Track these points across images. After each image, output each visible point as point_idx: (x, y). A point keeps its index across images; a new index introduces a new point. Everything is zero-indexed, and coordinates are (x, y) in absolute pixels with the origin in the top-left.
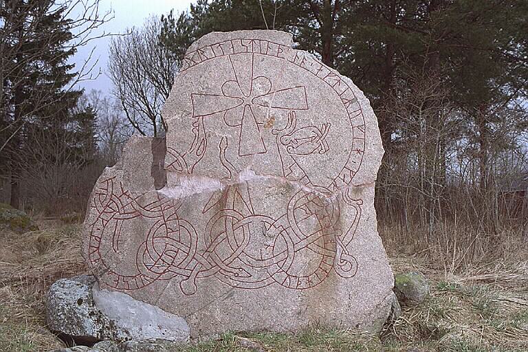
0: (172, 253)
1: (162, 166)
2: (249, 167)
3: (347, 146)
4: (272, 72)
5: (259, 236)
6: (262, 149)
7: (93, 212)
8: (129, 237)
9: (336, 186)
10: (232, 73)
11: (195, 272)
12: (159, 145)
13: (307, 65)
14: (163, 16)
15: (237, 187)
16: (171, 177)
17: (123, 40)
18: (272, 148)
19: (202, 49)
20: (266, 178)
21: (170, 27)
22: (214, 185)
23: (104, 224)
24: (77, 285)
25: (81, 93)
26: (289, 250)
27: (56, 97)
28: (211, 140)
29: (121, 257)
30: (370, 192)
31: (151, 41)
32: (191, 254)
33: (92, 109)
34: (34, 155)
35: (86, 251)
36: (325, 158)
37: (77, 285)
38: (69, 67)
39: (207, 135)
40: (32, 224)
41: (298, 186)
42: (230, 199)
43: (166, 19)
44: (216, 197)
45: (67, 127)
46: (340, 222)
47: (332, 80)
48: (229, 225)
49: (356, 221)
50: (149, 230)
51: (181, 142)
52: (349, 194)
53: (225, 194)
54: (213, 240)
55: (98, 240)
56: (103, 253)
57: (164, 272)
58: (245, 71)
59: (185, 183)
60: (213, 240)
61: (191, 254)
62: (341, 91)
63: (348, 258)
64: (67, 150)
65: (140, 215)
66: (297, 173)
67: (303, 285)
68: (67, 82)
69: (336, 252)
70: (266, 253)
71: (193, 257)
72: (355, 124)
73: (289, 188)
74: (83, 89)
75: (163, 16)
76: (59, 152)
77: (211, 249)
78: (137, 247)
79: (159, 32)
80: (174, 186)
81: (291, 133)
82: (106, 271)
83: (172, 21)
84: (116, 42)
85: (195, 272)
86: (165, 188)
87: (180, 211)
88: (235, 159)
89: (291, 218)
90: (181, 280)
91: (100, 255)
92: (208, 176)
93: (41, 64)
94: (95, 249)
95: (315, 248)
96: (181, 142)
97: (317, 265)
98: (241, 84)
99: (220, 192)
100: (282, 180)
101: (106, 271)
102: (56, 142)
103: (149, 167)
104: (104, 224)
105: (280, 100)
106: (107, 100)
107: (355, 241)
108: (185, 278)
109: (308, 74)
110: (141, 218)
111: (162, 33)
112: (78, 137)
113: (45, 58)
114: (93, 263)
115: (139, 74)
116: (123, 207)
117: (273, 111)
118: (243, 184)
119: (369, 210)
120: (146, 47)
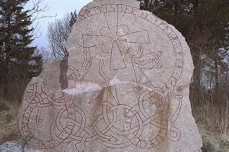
0: (71, 128)
1: (66, 76)
2: (116, 77)
3: (173, 64)
4: (129, 23)
5: (122, 117)
6: (123, 66)
7: (25, 103)
8: (46, 119)
9: (167, 87)
10: (106, 23)
11: (84, 138)
12: (64, 65)
13: (149, 18)
14: (72, 13)
15: (109, 88)
16: (71, 82)
17: (54, 24)
18: (129, 65)
19: (89, 10)
20: (126, 83)
21: (75, 18)
22: (96, 87)
23: (31, 110)
24: (16, 145)
25: (36, 48)
26: (140, 125)
27: (24, 49)
28: (94, 61)
29: (40, 129)
30: (187, 91)
31: (66, 24)
32: (82, 128)
33: (41, 55)
34: (14, 75)
35: (20, 126)
36: (160, 71)
37: (16, 145)
38: (31, 36)
39: (92, 58)
40: (7, 107)
41: (145, 88)
42: (105, 95)
43: (73, 14)
44: (97, 94)
45: (30, 63)
46: (170, 109)
47: (163, 27)
48: (105, 111)
49: (179, 108)
50: (57, 113)
51: (76, 62)
52: (175, 92)
53: (102, 92)
54: (95, 119)
55: (28, 119)
56: (30, 127)
57: (66, 138)
58: (113, 22)
59: (79, 85)
60: (95, 119)
61: (82, 128)
62: (168, 33)
63: (175, 130)
64: (29, 73)
65: (52, 105)
66: (144, 80)
67: (149, 146)
68: (30, 43)
69: (168, 126)
70: (127, 127)
71: (83, 129)
72: (177, 51)
73: (139, 88)
74: (37, 46)
75: (72, 13)
76: (25, 74)
77: (94, 125)
78: (50, 123)
79: (70, 20)
80: (72, 88)
81: (141, 57)
82: (32, 138)
83: (76, 15)
84: (51, 24)
85: (84, 138)
86: (67, 89)
87: (76, 102)
88: (108, 72)
89: (141, 106)
90: (76, 143)
91: (28, 128)
92: (92, 82)
93: (18, 36)
94: (26, 125)
95: (155, 124)
96: (76, 62)
97: (156, 134)
98: (111, 29)
99: (99, 91)
100: (135, 84)
101: (32, 138)
102: (24, 70)
103: (58, 77)
104: (31, 110)
105: (133, 38)
106: (48, 52)
107: (179, 120)
108: (78, 142)
109: (149, 23)
110: (53, 107)
111: (71, 20)
112: (34, 67)
113: (20, 32)
114: (25, 133)
115: (61, 39)
116: (42, 100)
117: (129, 44)
118: (112, 86)
119: (186, 101)
120: (64, 27)
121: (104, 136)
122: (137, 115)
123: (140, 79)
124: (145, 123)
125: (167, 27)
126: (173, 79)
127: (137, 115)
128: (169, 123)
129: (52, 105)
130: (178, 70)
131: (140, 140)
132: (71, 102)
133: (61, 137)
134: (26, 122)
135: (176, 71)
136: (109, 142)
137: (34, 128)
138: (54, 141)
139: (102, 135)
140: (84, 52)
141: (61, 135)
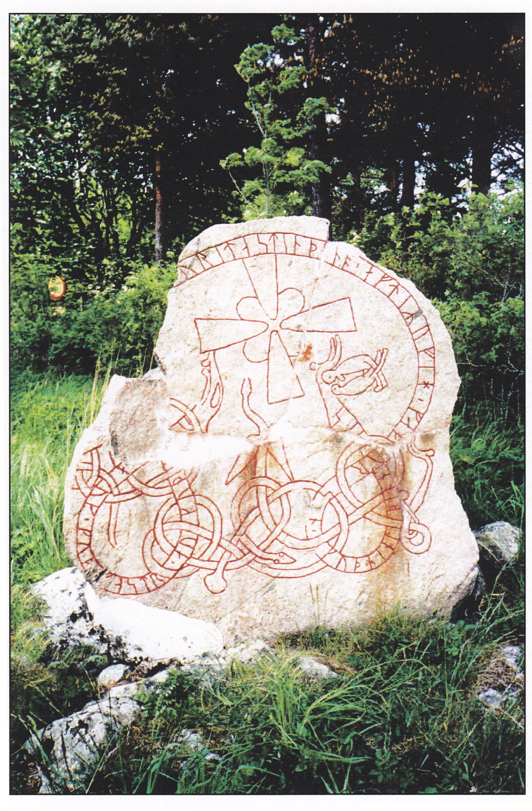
18: (312, 389)
32: (216, 540)
42: (260, 464)
44: (242, 461)
48: (262, 498)
49: (427, 479)
53: (254, 458)
55: (88, 533)
57: (182, 568)
61: (216, 540)
63: (420, 528)
66: (346, 420)
67: (364, 567)
72: (421, 346)
74: (163, 465)
77: (242, 530)
95: (375, 518)
101: (102, 573)
114: (85, 565)
116: (117, 486)
121: (265, 556)
122: (334, 501)
123: (336, 419)
124: (352, 518)
125: (396, 287)
126: (412, 414)
127: (334, 501)
128: (406, 514)
129: (141, 494)
130: (424, 393)
131: (343, 556)
132: (184, 485)
133: (169, 565)
134: (85, 539)
135: (418, 395)
136: (277, 566)
137: (105, 551)
138: (156, 575)
139: (260, 554)
140: (206, 364)
141: (169, 562)
